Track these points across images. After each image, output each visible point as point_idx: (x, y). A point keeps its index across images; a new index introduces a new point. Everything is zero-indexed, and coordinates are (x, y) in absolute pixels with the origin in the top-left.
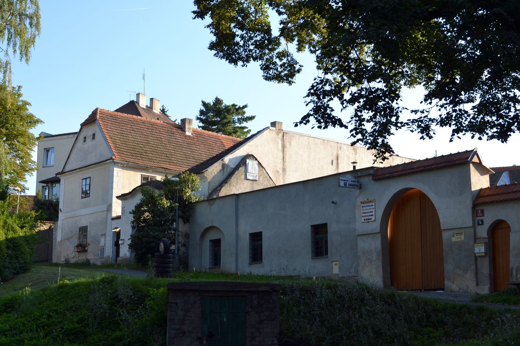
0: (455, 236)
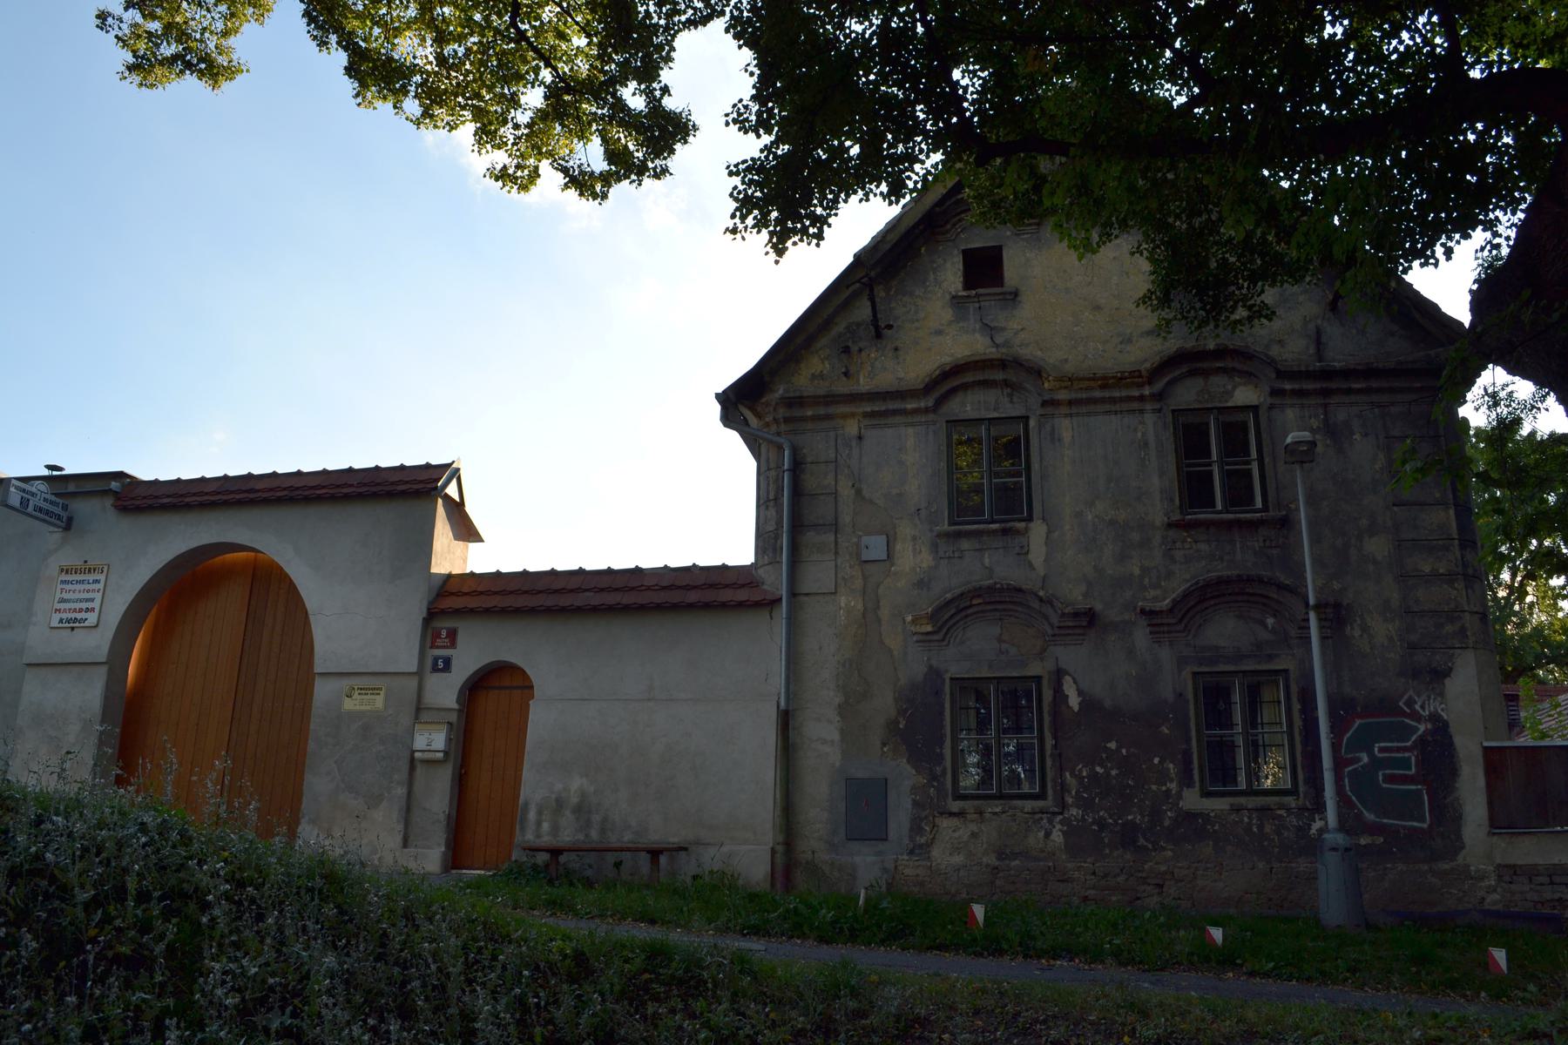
0: (356, 695)
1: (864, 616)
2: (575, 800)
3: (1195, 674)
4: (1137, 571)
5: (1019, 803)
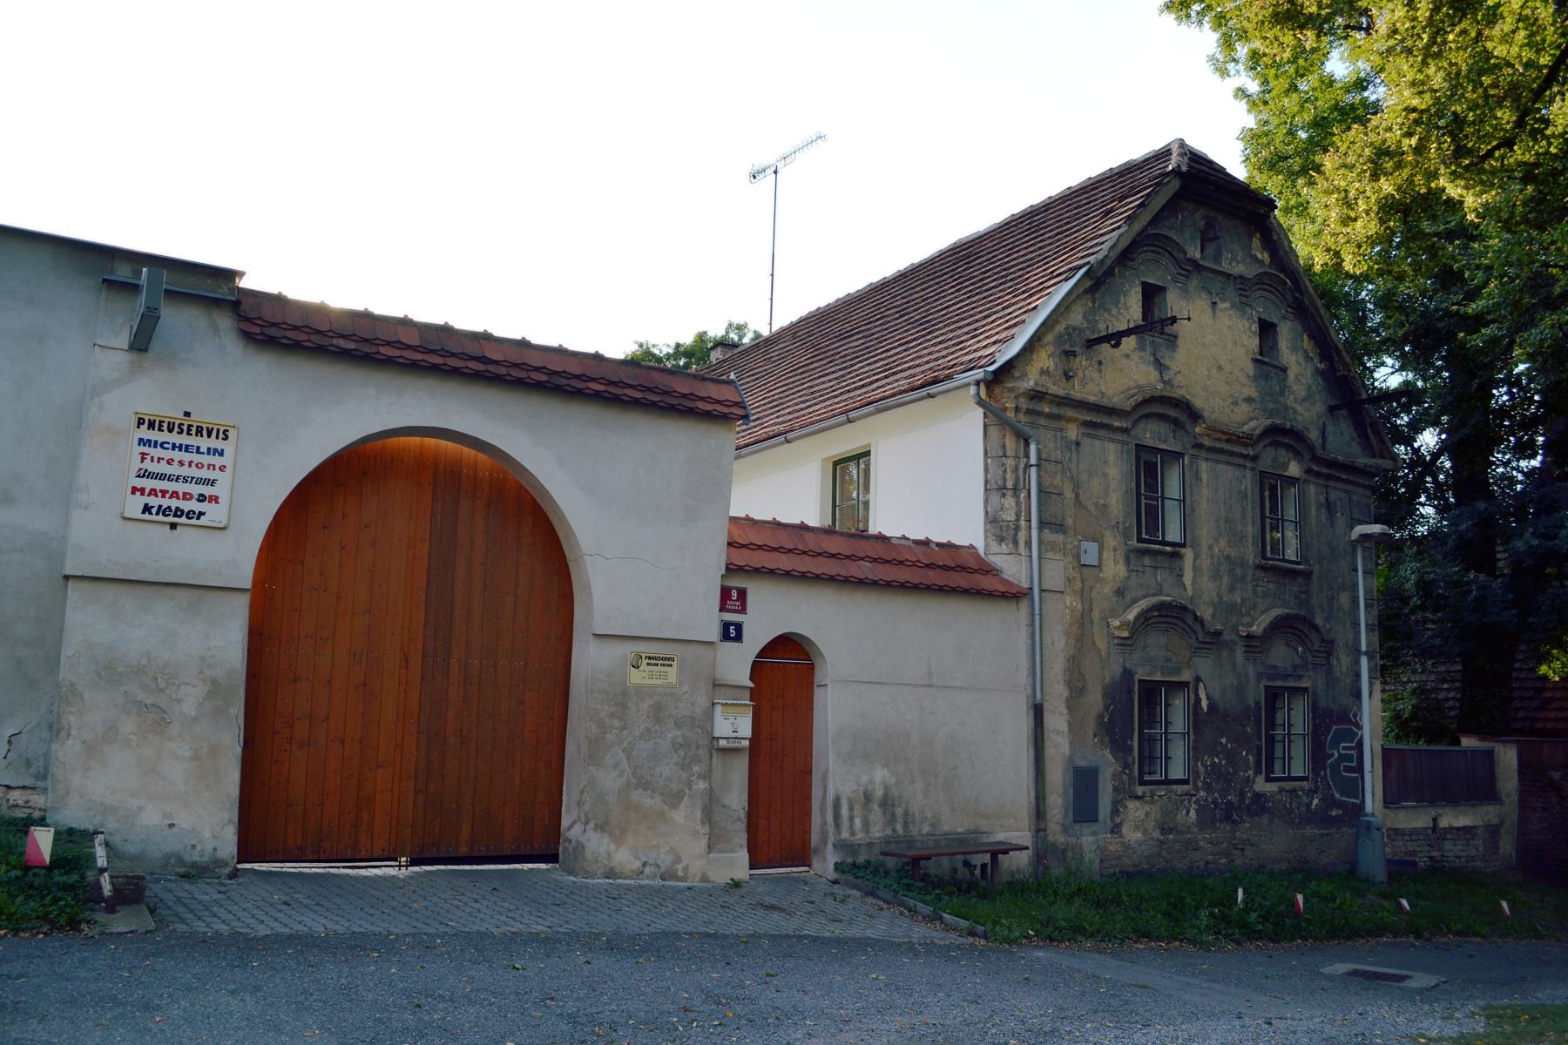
0: (644, 666)
1: (1082, 618)
2: (880, 793)
3: (1266, 687)
4: (1239, 601)
5: (1175, 787)
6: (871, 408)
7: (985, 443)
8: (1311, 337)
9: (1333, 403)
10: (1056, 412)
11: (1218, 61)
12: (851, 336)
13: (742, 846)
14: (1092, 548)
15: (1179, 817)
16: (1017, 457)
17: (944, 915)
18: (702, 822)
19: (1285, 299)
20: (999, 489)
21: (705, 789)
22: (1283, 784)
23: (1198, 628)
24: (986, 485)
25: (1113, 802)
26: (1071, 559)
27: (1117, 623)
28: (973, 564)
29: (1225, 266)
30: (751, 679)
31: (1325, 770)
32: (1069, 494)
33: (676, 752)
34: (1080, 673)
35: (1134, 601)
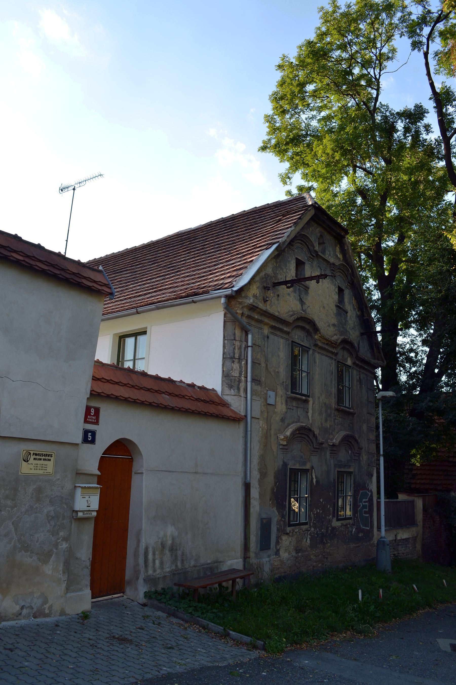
0: (31, 461)
1: (267, 433)
2: (170, 542)
3: (338, 471)
4: (329, 426)
5: (302, 526)
6: (153, 306)
7: (224, 331)
8: (356, 299)
9: (362, 331)
10: (260, 318)
11: (283, 176)
12: (121, 272)
13: (87, 586)
14: (271, 394)
15: (303, 543)
16: (241, 341)
17: (231, 632)
18: (64, 573)
19: (348, 279)
20: (231, 358)
21: (67, 548)
22: (343, 522)
23: (314, 440)
24: (223, 355)
25: (277, 537)
26: (263, 400)
27: (282, 437)
28: (217, 400)
29: (326, 257)
30: (99, 469)
31: (357, 514)
32: (263, 365)
33: (49, 523)
34: (265, 465)
35: (289, 425)
